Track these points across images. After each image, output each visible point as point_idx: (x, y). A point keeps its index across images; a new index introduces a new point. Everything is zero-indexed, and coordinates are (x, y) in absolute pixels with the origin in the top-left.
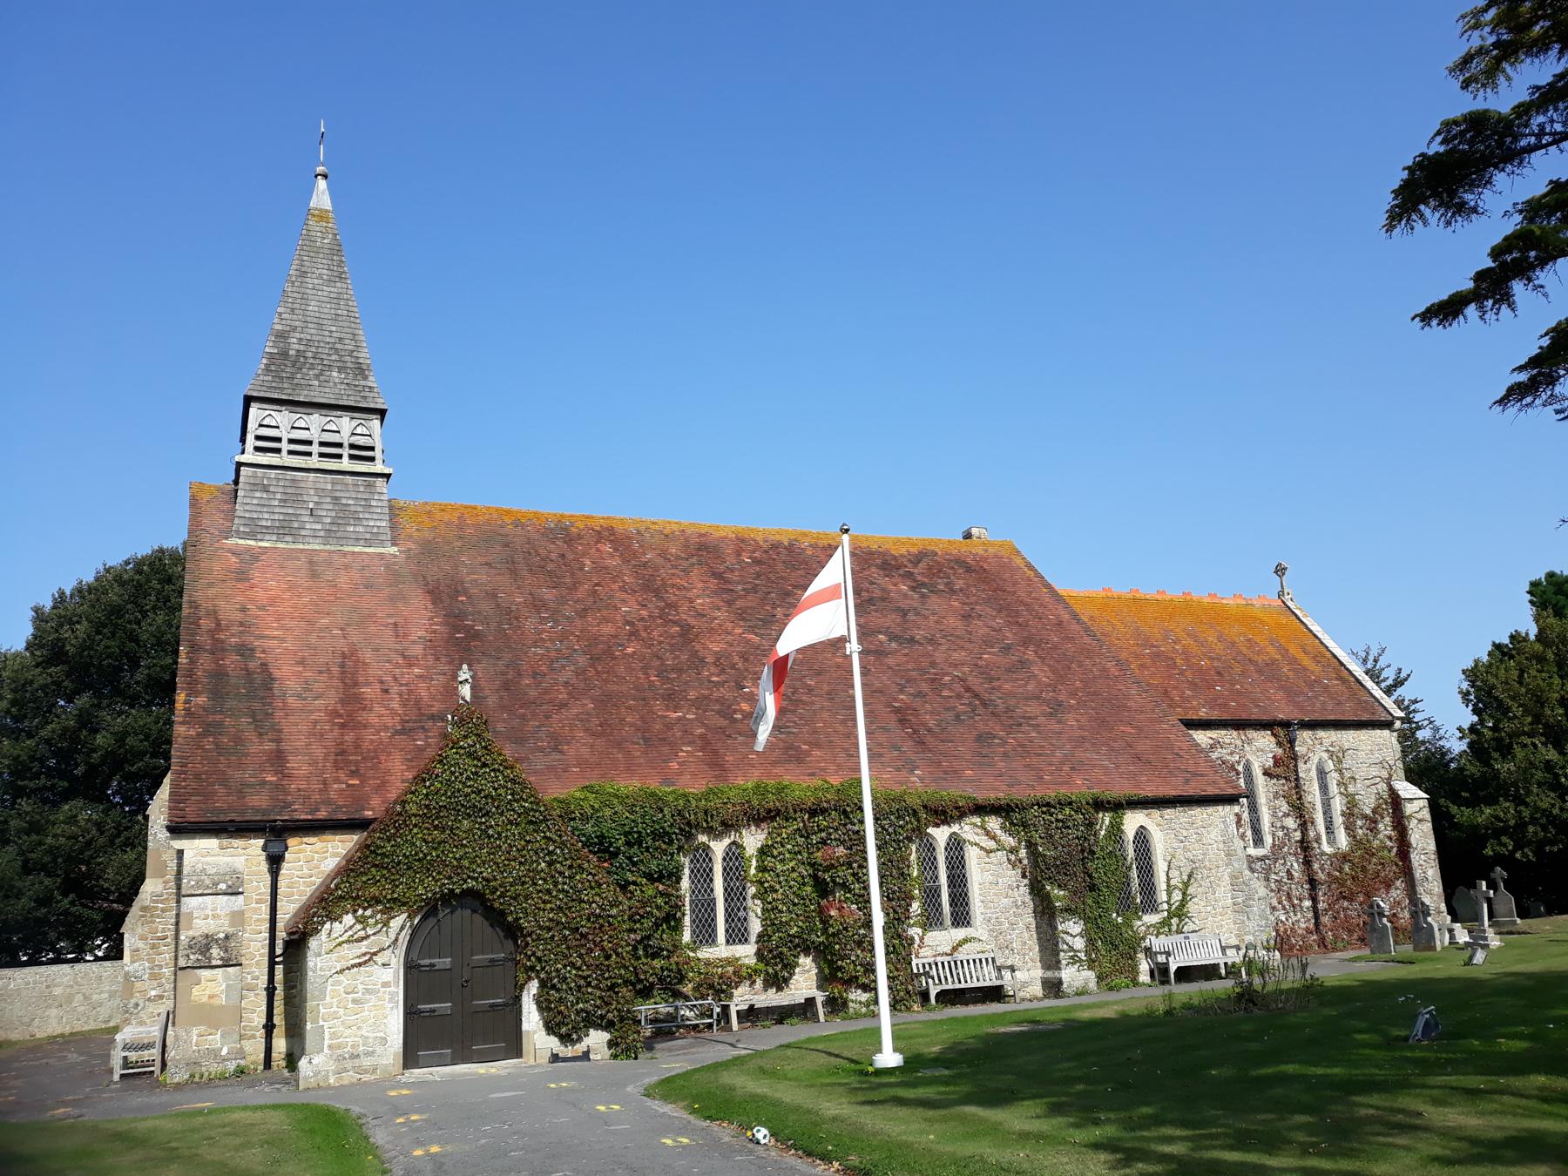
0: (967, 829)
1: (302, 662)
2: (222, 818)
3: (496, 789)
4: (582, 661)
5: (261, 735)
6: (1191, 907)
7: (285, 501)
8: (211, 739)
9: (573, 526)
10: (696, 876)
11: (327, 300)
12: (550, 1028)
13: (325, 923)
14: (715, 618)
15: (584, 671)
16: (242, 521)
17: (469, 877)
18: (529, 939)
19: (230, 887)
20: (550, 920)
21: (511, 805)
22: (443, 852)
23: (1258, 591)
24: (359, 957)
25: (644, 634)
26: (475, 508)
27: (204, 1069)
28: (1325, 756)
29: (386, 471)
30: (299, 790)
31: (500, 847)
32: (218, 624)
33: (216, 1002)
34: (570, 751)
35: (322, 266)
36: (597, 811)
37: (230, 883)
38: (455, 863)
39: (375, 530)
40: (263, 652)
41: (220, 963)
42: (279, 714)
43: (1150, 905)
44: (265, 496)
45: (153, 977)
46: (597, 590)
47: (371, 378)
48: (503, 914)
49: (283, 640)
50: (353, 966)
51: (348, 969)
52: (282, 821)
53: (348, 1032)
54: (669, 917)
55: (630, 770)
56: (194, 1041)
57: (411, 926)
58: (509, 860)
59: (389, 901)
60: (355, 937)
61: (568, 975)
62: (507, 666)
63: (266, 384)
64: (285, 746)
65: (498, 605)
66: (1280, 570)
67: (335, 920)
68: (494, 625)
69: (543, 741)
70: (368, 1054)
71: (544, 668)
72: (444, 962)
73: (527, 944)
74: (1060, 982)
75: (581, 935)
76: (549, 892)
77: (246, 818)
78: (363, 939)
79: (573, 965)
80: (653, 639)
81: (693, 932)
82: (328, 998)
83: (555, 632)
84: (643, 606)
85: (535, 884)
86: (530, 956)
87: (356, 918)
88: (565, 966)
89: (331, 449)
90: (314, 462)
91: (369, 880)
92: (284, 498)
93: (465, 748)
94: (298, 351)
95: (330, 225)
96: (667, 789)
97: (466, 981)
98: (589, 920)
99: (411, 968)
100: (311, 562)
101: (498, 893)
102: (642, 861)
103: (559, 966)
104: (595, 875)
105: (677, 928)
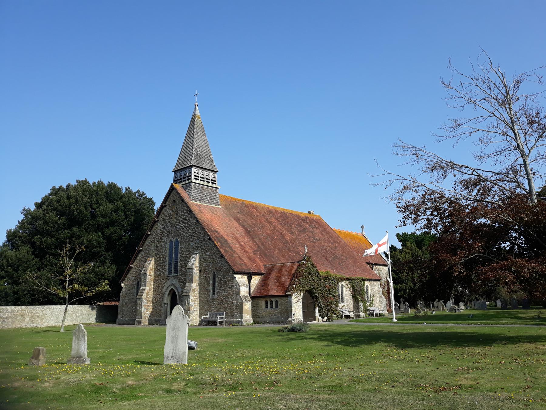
0: (343, 283)
6: (374, 302)
12: (320, 315)
23: (359, 231)
26: (226, 196)
28: (377, 271)
43: (368, 301)
45: (195, 306)
66: (362, 227)
74: (360, 315)
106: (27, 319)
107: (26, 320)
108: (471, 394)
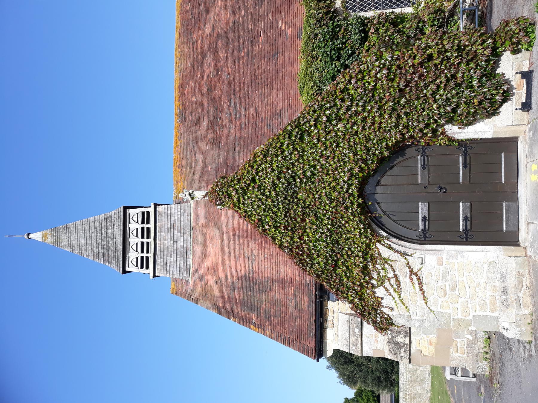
1: (238, 258)
2: (313, 327)
3: (273, 170)
4: (235, 100)
5: (270, 290)
7: (171, 255)
8: (273, 318)
9: (179, 108)
10: (365, 7)
11: (79, 234)
13: (382, 312)
14: (214, 19)
15: (240, 98)
16: (181, 276)
17: (347, 192)
18: (407, 136)
19: (357, 326)
20: (390, 117)
21: (286, 157)
22: (324, 215)
24: (413, 284)
25: (222, 62)
26: (175, 159)
27: (481, 351)
29: (153, 206)
30: (299, 275)
31: (322, 165)
32: (222, 297)
33: (434, 341)
34: (281, 104)
35: (65, 236)
36: (315, 83)
37: (355, 326)
38: (334, 204)
39: (182, 211)
40: (233, 277)
41: (408, 339)
42: (260, 277)
44: (169, 264)
46: (204, 93)
47: (110, 214)
48: (381, 160)
49: (228, 265)
50: (422, 290)
51: (423, 294)
52: (315, 291)
53: (480, 295)
54: (394, 24)
55: (291, 63)
56: (461, 355)
57: (388, 239)
58: (334, 158)
59: (365, 259)
60: (395, 286)
61: (444, 97)
62: (238, 144)
63: (117, 264)
64: (276, 278)
65: (212, 149)
67: (380, 303)
68: (221, 152)
69: (275, 123)
70: (504, 278)
71: (239, 123)
72: (423, 209)
73: (412, 137)
75: (407, 86)
76: (364, 120)
77: (314, 313)
78: (398, 281)
79: (434, 93)
80: (224, 56)
81: (406, 5)
82: (448, 311)
83: (222, 116)
84: (209, 65)
85: (357, 132)
86: (423, 134)
87: (378, 286)
88: (435, 101)
89: (145, 233)
90: (151, 241)
91: (346, 275)
92: (169, 255)
93: (239, 197)
94: (102, 248)
95: (48, 232)
96: (303, 34)
97: (441, 190)
98: (393, 80)
99: (425, 237)
100: (197, 244)
101: (363, 165)
102: (352, 47)
103: (435, 106)
104: (351, 77)
105: (402, 18)
106: (419, 389)
107: (420, 392)
108: (280, 282)
